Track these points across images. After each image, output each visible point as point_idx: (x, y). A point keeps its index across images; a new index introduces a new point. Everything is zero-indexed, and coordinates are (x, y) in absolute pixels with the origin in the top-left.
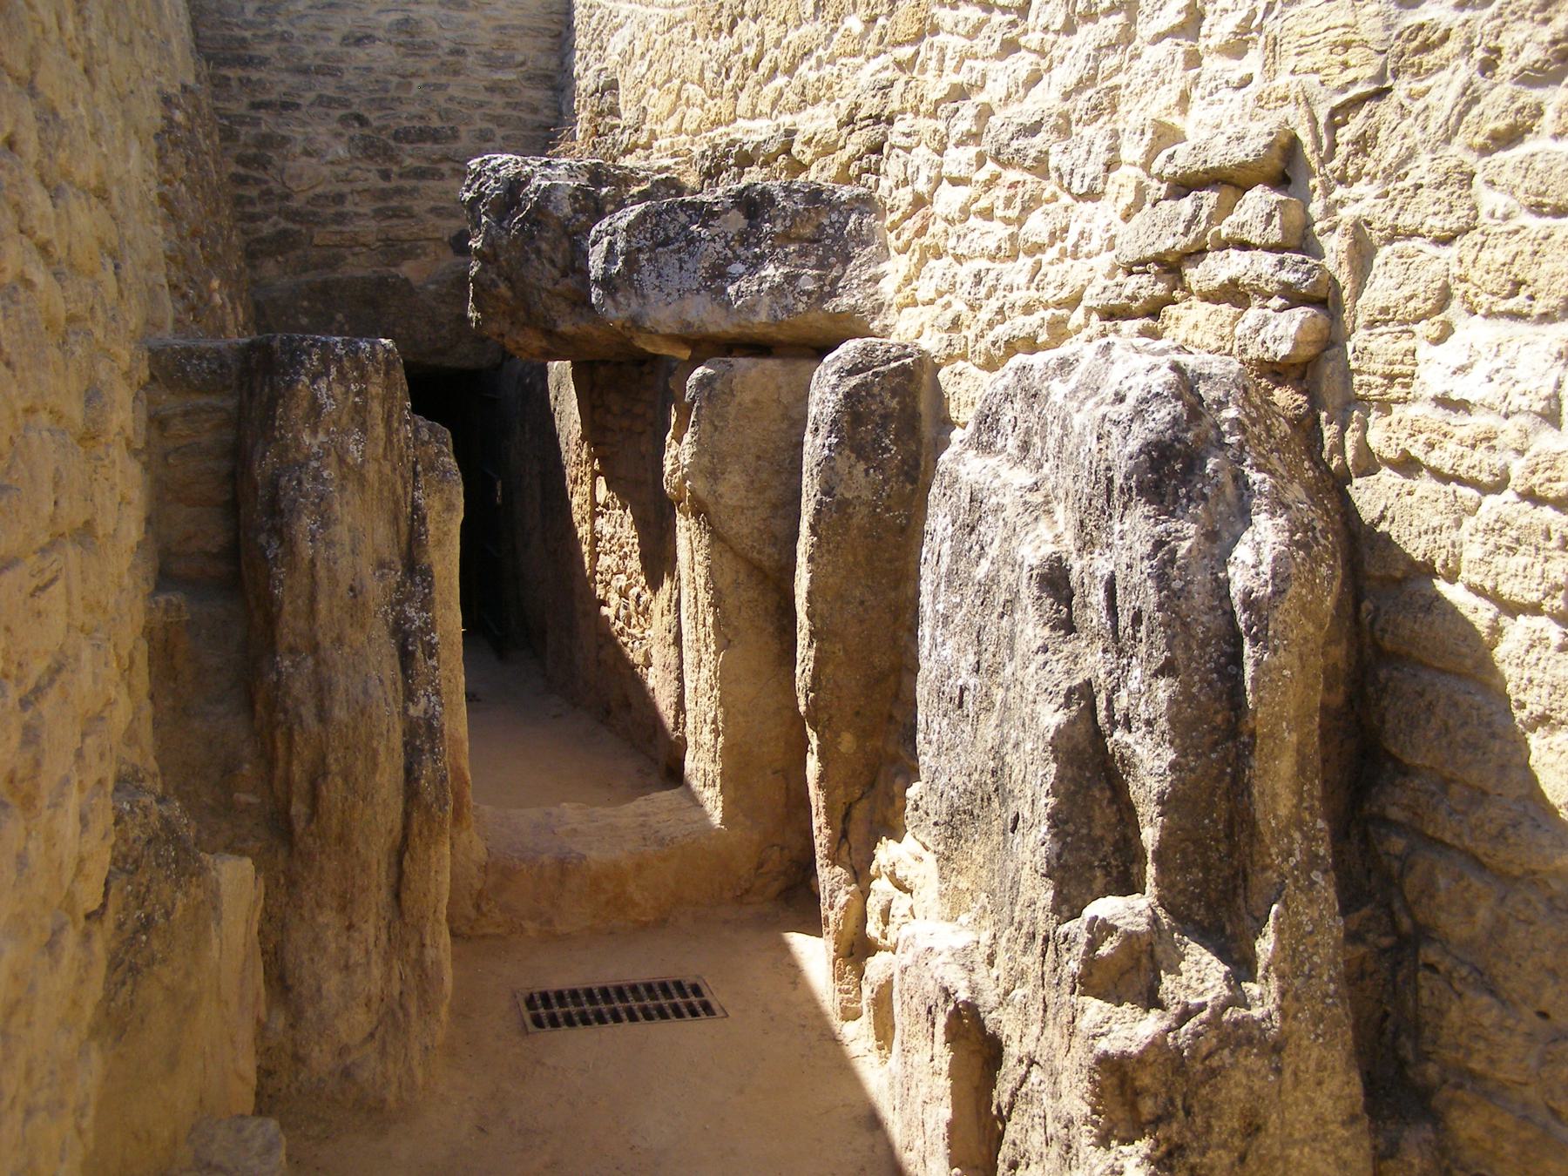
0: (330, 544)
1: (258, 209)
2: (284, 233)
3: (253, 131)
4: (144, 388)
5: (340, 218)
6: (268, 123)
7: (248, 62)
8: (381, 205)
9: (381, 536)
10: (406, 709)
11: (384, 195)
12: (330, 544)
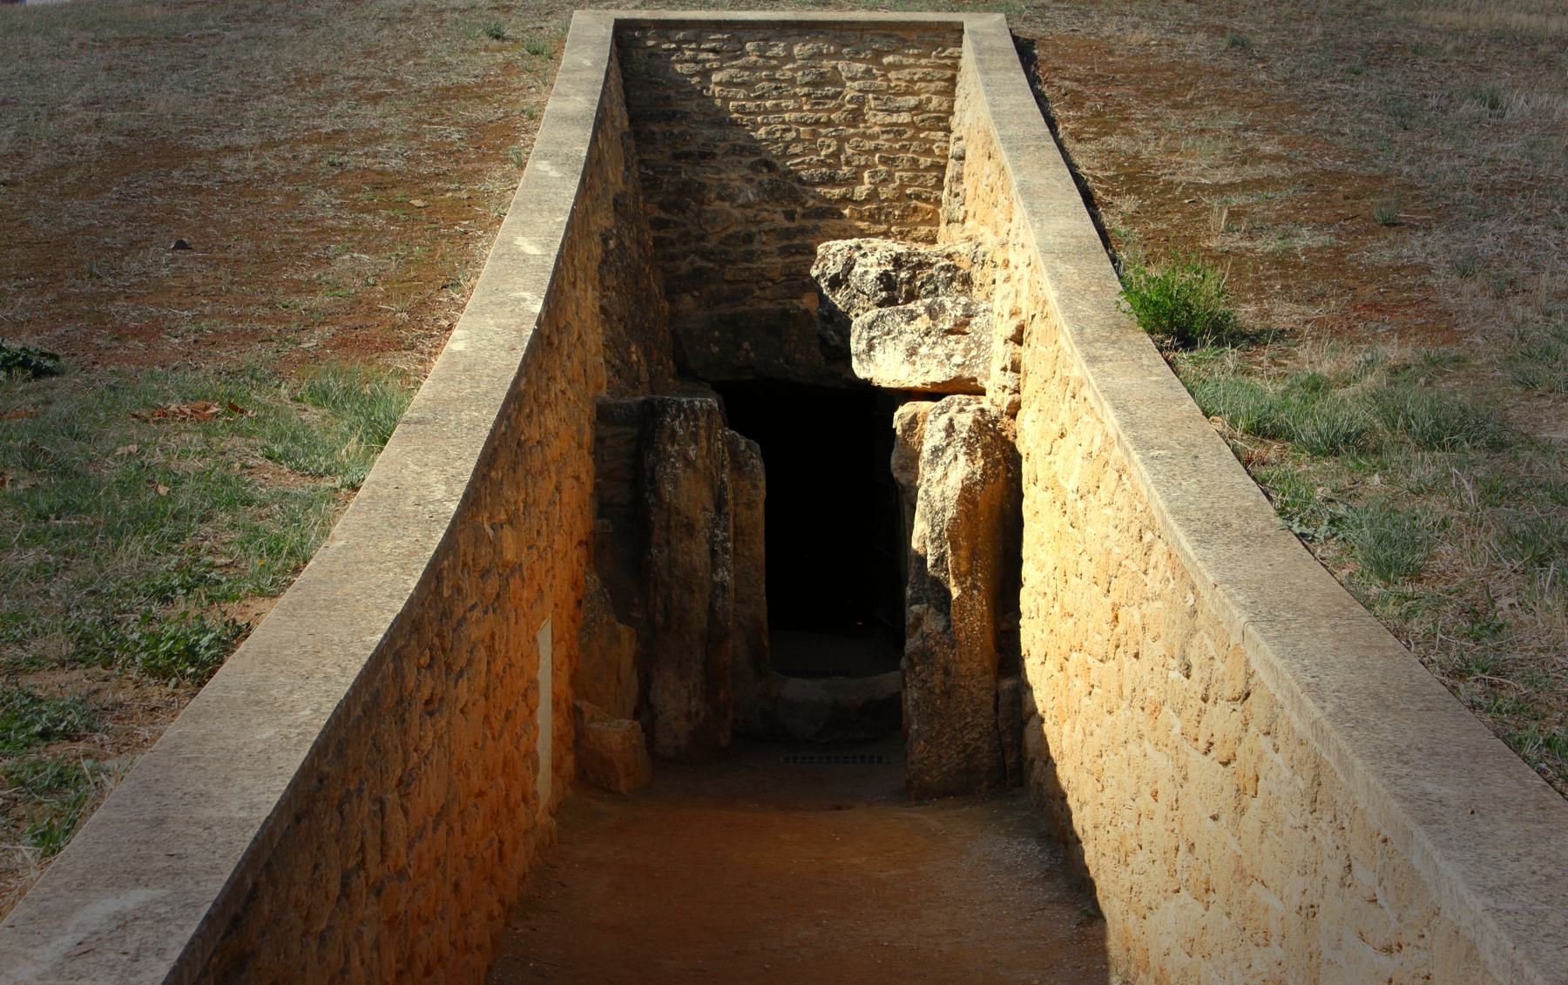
7: (670, 117)
9: (705, 495)
11: (788, 234)
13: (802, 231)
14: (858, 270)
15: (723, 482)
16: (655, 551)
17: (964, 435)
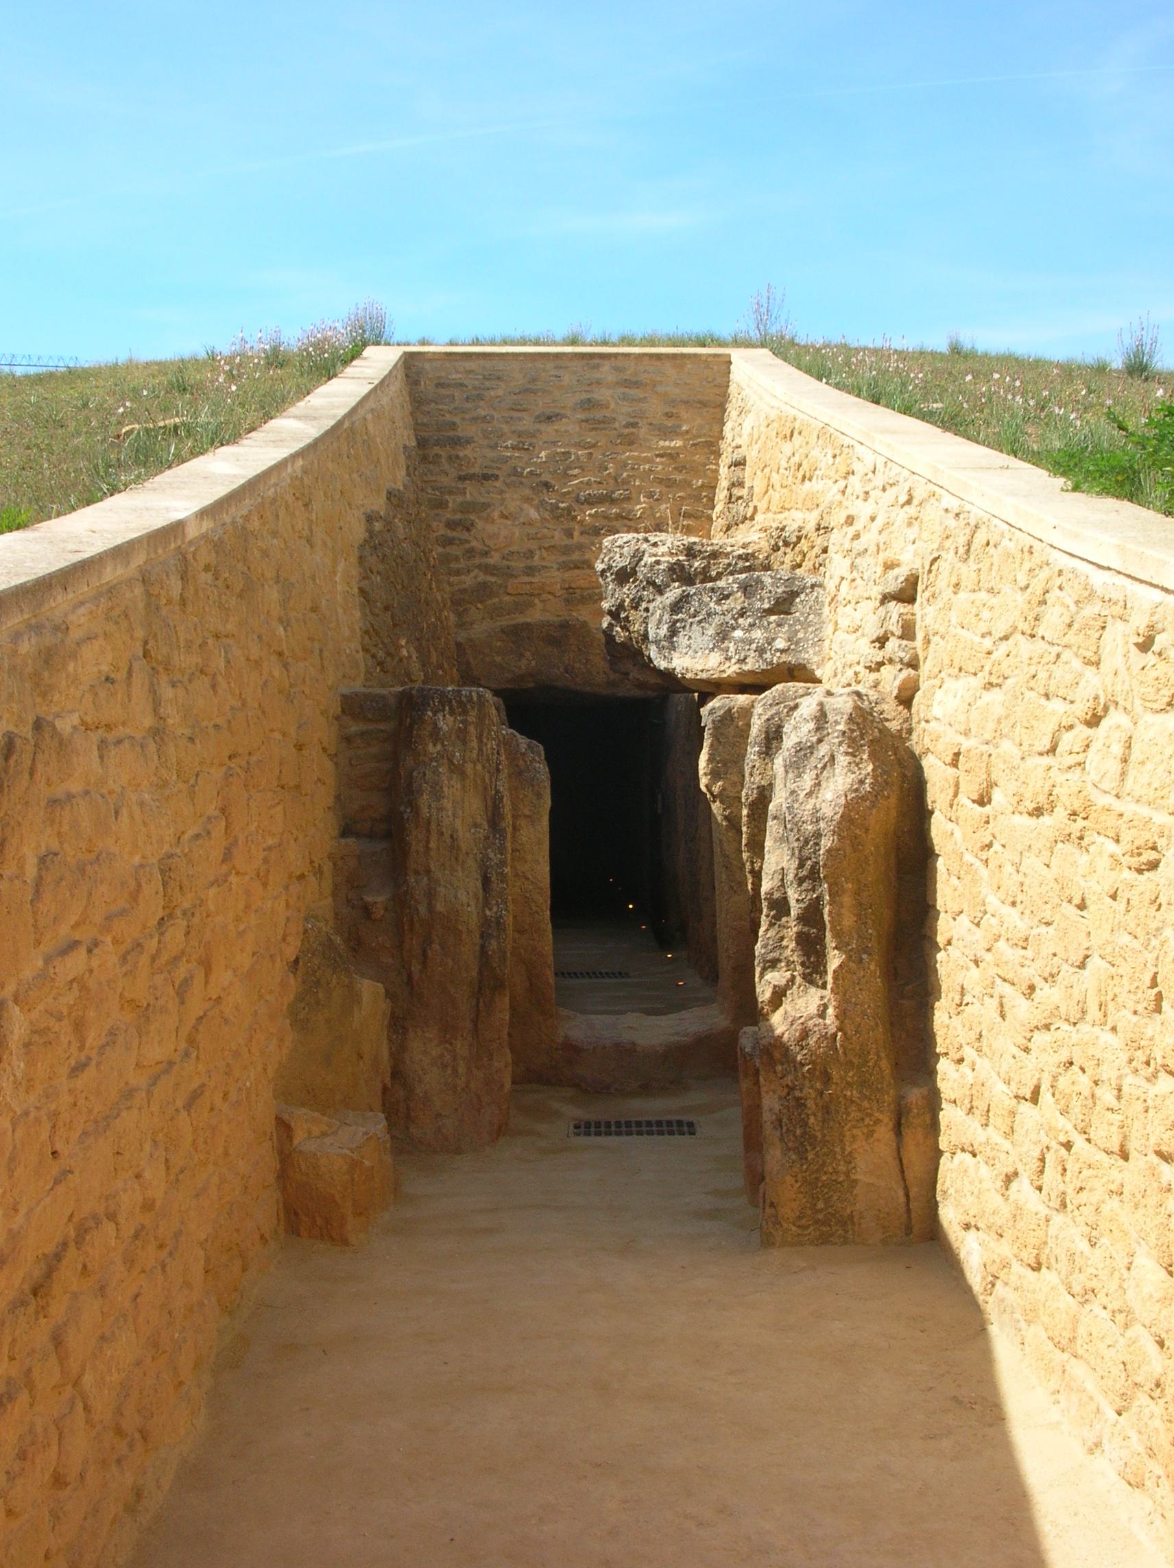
0: (440, 809)
1: (462, 564)
2: (484, 586)
3: (459, 499)
4: (337, 718)
5: (530, 571)
6: (472, 492)
7: (457, 442)
8: (564, 558)
9: (475, 805)
10: (483, 911)
11: (567, 550)
12: (440, 809)
13: (580, 547)
14: (648, 560)
15: (497, 792)
16: (412, 880)
17: (841, 727)
